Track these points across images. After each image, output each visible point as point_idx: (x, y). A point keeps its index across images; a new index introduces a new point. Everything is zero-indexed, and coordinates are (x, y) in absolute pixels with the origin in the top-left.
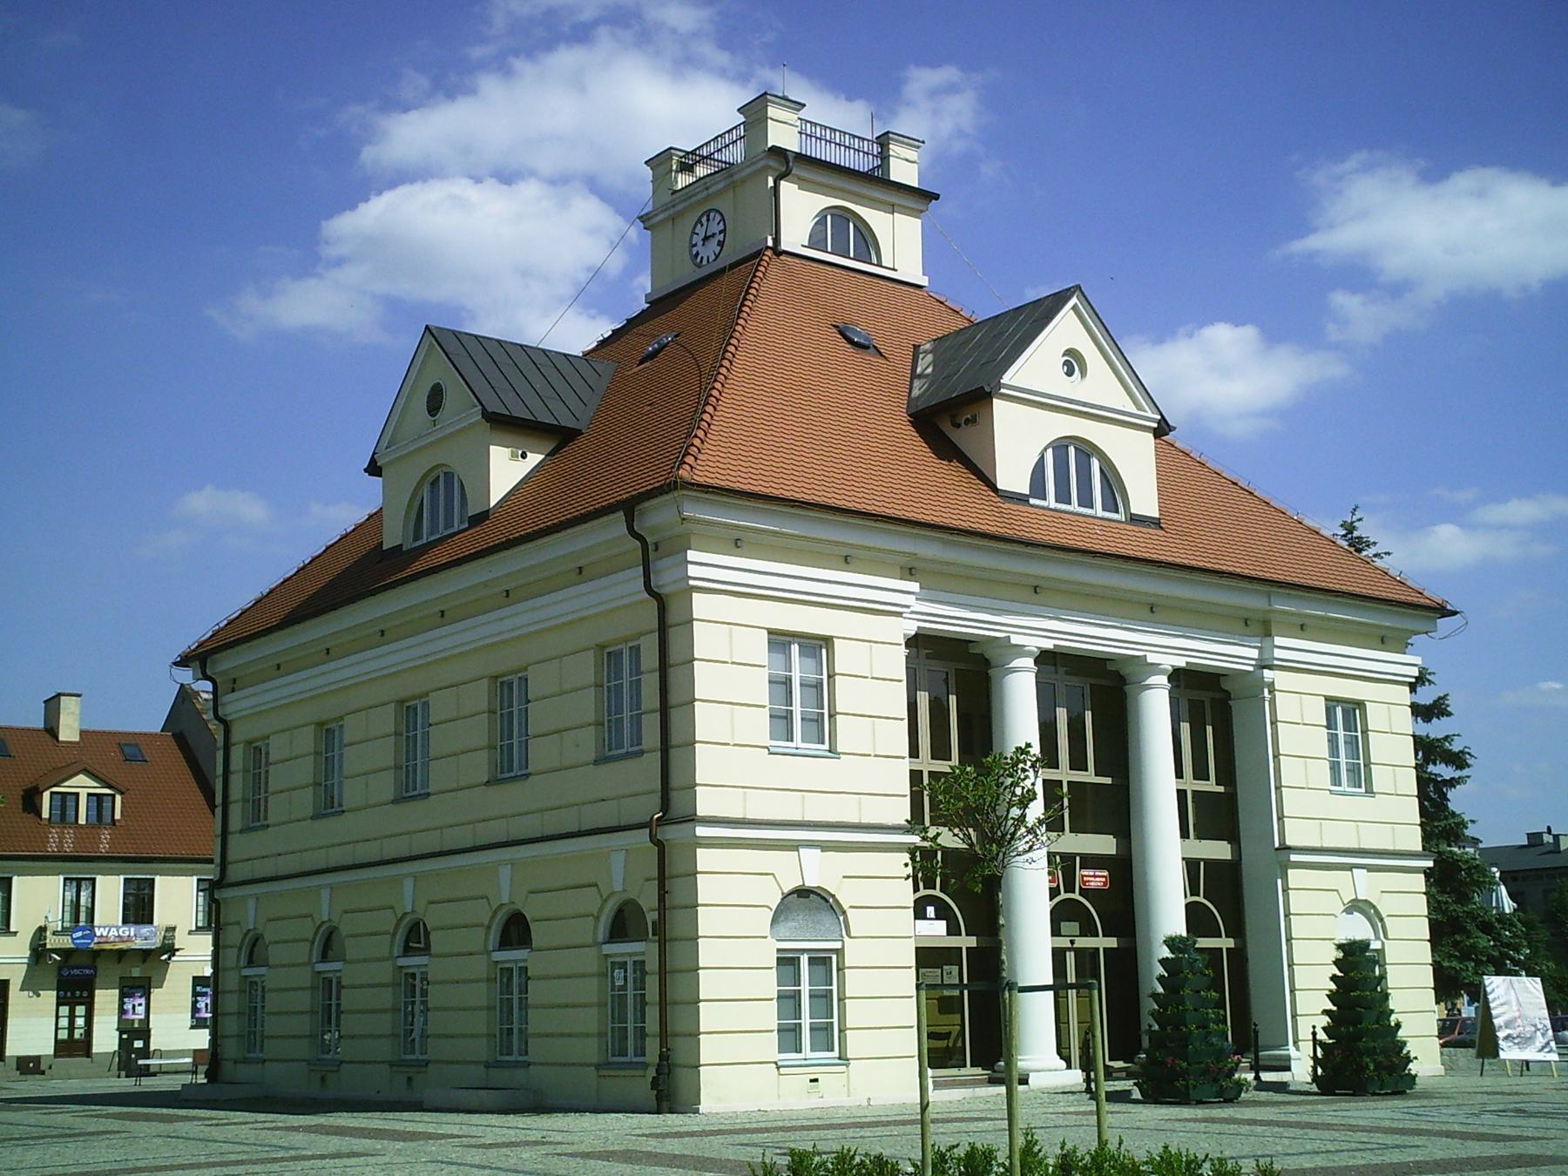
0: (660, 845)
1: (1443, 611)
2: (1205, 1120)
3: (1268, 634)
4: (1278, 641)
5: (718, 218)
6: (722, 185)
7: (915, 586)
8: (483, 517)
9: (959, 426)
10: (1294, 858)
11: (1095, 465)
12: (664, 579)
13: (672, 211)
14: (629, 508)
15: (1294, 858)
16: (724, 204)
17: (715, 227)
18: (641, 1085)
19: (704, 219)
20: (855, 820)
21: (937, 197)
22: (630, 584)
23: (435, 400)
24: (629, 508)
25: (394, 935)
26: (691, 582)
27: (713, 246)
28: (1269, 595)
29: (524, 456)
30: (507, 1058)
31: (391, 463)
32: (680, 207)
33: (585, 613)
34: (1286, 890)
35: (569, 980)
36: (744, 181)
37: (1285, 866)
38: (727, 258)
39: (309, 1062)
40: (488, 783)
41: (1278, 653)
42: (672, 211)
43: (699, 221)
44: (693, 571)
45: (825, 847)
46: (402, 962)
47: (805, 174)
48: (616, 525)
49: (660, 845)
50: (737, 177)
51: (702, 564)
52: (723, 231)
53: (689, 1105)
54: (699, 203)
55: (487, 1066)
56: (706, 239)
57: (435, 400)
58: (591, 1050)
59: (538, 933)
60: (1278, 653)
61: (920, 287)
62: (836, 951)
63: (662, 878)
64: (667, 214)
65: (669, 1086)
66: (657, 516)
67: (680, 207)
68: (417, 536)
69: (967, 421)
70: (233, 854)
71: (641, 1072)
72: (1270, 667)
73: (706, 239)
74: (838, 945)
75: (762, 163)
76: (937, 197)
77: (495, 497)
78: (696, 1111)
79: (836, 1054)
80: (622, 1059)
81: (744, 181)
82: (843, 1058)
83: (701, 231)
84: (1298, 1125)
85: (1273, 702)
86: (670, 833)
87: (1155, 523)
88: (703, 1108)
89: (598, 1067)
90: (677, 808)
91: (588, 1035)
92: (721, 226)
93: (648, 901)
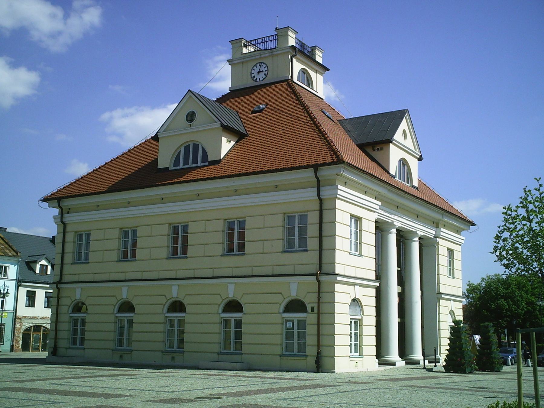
0: (319, 282)
1: (473, 224)
2: (204, 374)
3: (437, 227)
4: (443, 230)
5: (264, 66)
6: (267, 55)
7: (379, 203)
8: (218, 162)
9: (374, 150)
10: (443, 296)
11: (406, 167)
12: (326, 193)
13: (243, 60)
14: (316, 167)
15: (443, 296)
16: (268, 61)
17: (263, 68)
18: (311, 361)
19: (258, 65)
20: (354, 275)
21: (328, 70)
22: (312, 193)
23: (191, 117)
24: (316, 167)
25: (164, 305)
26: (338, 196)
27: (262, 76)
28: (443, 215)
29: (230, 142)
30: (120, 348)
31: (162, 137)
32: (247, 59)
33: (279, 202)
34: (439, 306)
35: (264, 325)
36: (277, 55)
37: (439, 299)
38: (266, 81)
39: (113, 350)
40: (221, 255)
41: (442, 233)
42: (243, 60)
43: (255, 65)
44: (339, 192)
45: (455, 301)
46: (167, 315)
47: (301, 58)
48: (309, 173)
49: (319, 282)
50: (274, 53)
51: (343, 191)
52: (267, 71)
53: (331, 370)
54: (258, 59)
55: (218, 354)
56: (259, 72)
57: (191, 117)
58: (278, 350)
59: (245, 308)
60: (442, 233)
61: (322, 99)
62: (359, 319)
63: (319, 293)
64: (241, 61)
65: (322, 363)
66: (325, 173)
67: (247, 59)
68: (177, 162)
69: (378, 149)
70: (65, 272)
71: (304, 358)
72: (438, 237)
73: (259, 72)
74: (360, 318)
75: (287, 50)
76: (328, 70)
77: (222, 156)
78: (334, 372)
79: (358, 354)
80: (292, 353)
81: (277, 55)
82: (361, 355)
83: (257, 69)
84: (275, 378)
85: (438, 248)
86: (322, 278)
87: (417, 188)
88: (337, 370)
89: (280, 356)
90: (325, 268)
91: (277, 345)
92: (266, 69)
93: (310, 300)
